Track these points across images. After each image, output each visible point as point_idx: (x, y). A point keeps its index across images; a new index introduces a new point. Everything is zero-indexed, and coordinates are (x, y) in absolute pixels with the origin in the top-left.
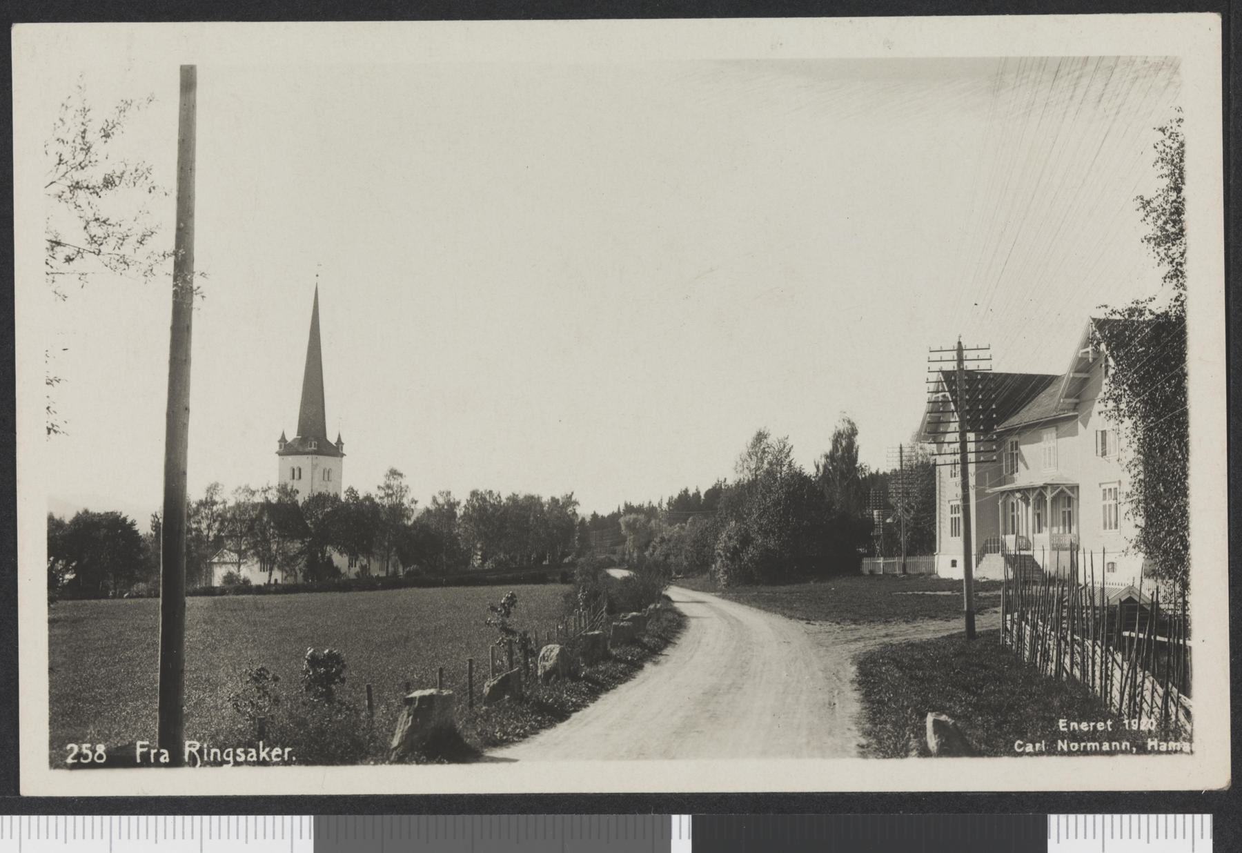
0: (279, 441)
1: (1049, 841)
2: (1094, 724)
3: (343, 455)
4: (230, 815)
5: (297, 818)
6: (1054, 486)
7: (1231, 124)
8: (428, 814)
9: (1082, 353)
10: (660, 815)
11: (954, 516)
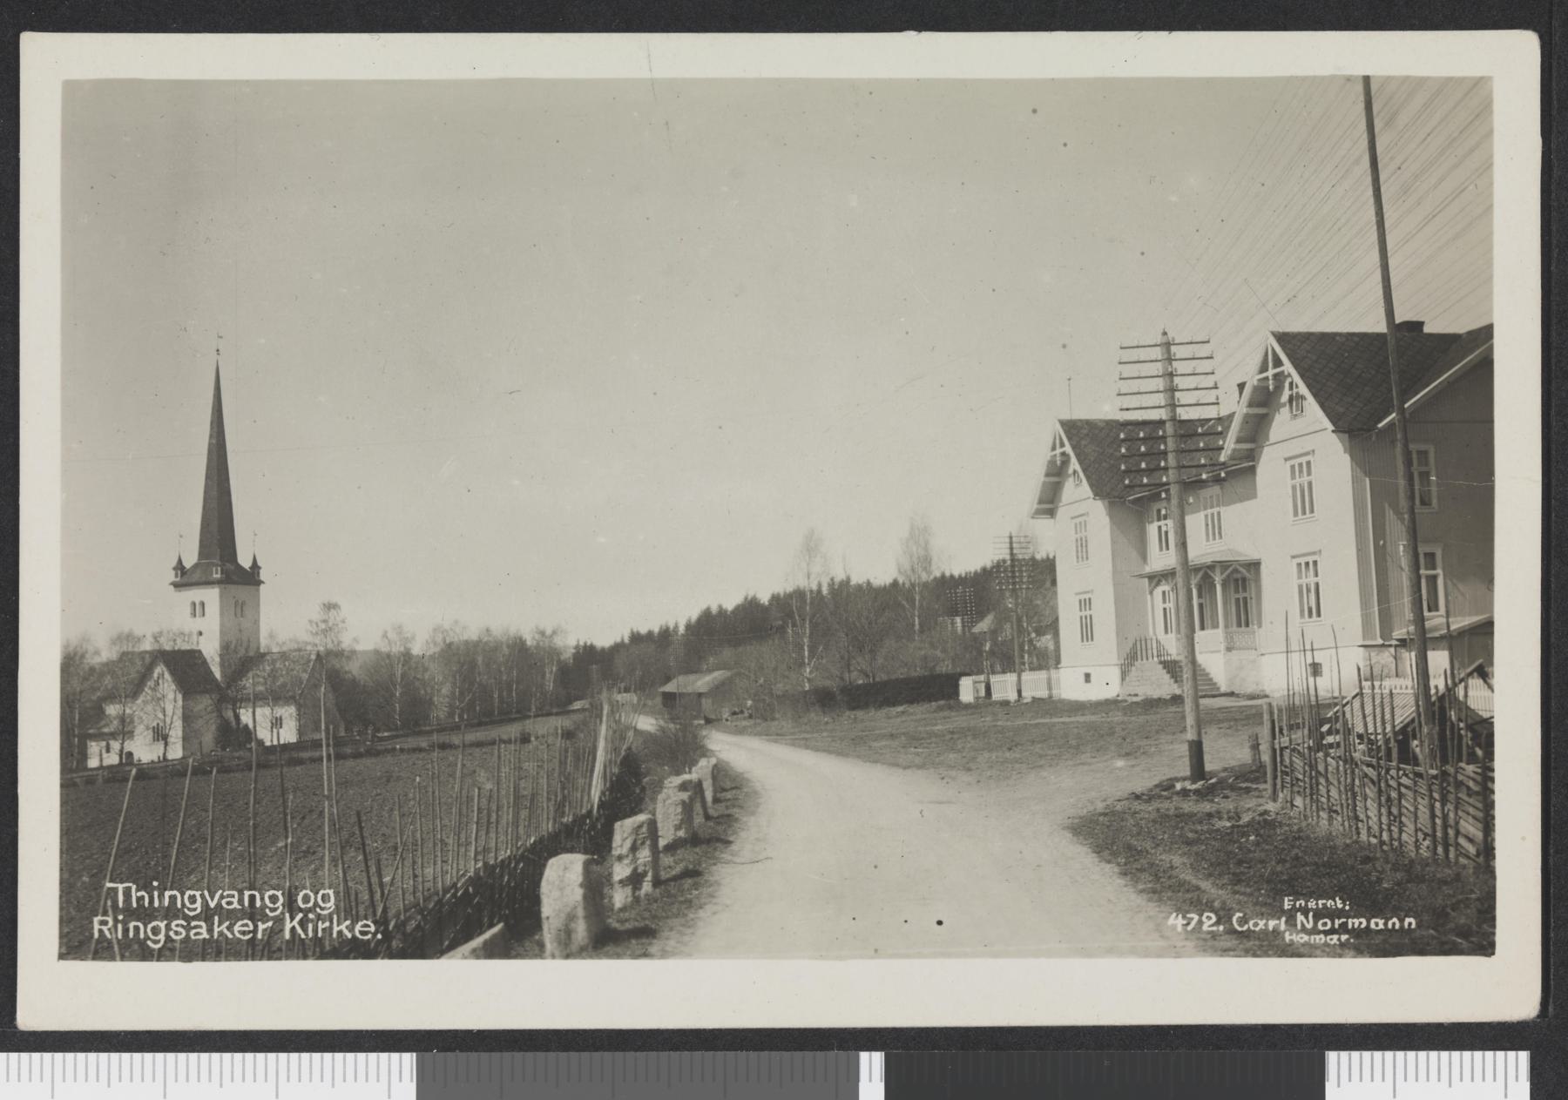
0: (174, 569)
5: (395, 1056)
6: (1224, 565)
9: (1259, 380)
11: (1083, 613)
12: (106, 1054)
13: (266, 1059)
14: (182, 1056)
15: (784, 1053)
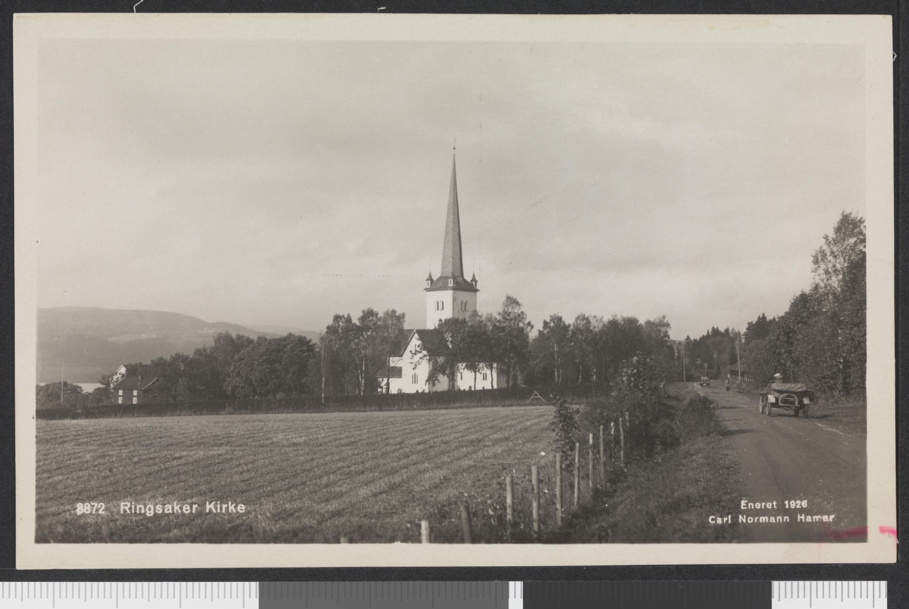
1: (773, 600)
2: (764, 504)
3: (476, 291)
7: (900, 98)
8: (339, 581)
10: (501, 582)
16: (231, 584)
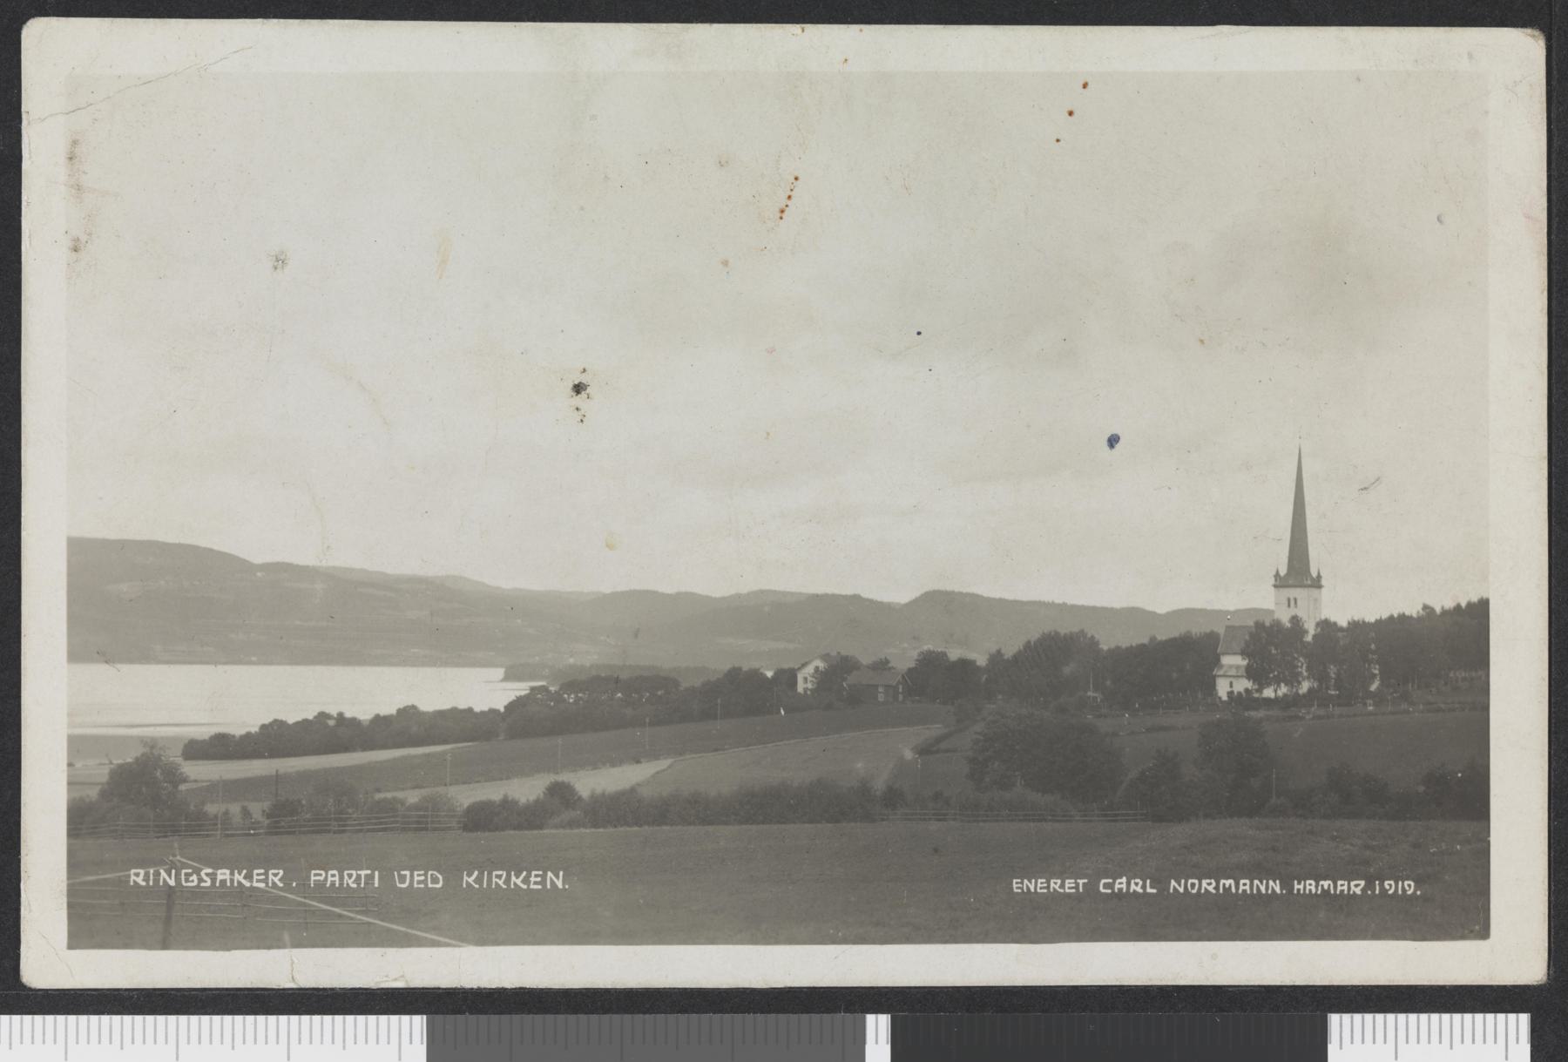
1: (1330, 1047)
4: (324, 1014)
8: (567, 1013)
12: (119, 1017)
13: (144, 1021)
14: (194, 1019)
15: (791, 1015)
16: (378, 1019)
